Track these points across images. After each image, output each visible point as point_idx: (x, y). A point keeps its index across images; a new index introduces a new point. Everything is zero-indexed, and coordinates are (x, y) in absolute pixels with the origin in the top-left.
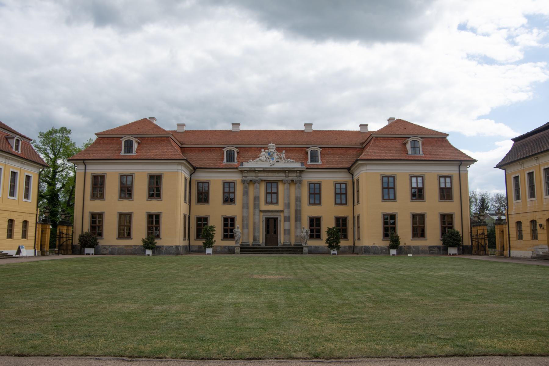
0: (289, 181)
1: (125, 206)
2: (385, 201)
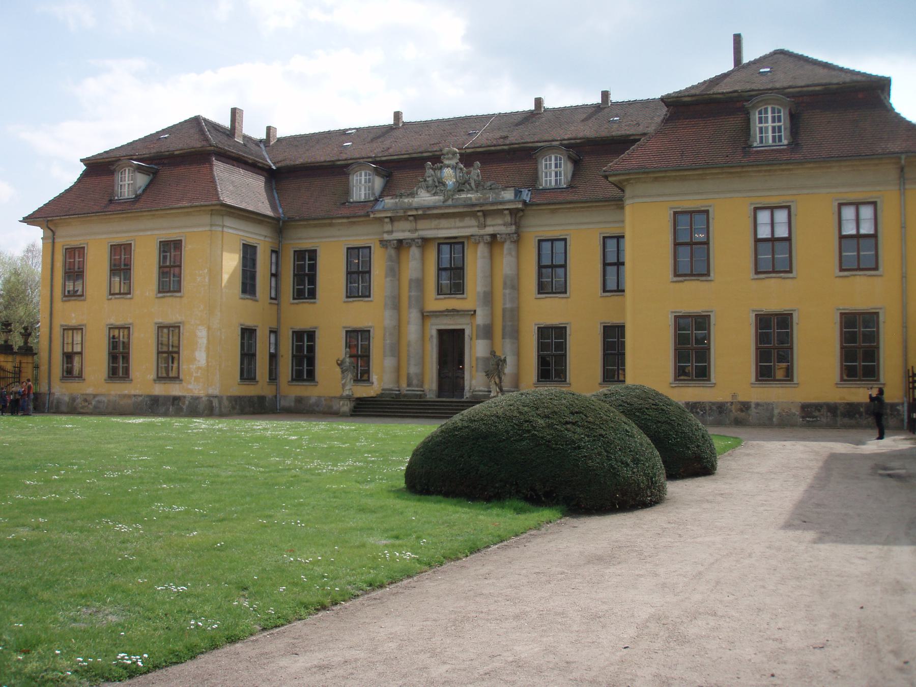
2: (680, 279)
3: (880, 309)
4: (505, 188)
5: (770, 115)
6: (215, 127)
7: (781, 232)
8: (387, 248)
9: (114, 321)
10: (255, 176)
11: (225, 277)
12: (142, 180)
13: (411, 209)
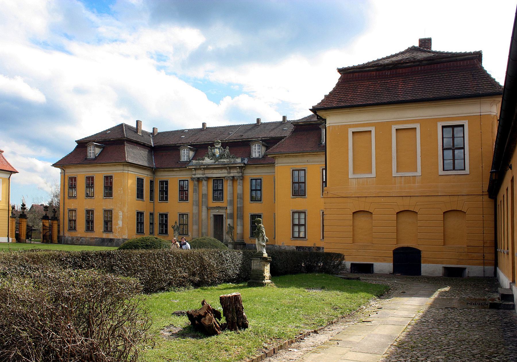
2: (295, 197)
6: (129, 128)
12: (98, 151)
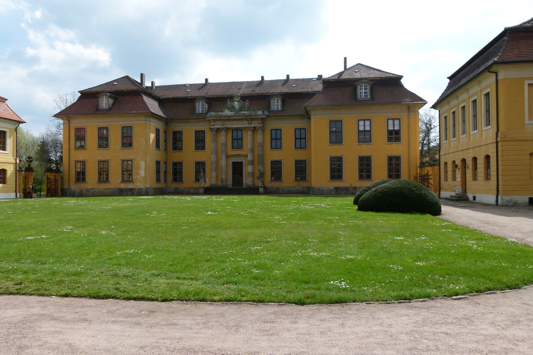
0: (251, 128)
1: (103, 154)
2: (332, 144)
3: (401, 155)
4: (259, 110)
5: (364, 87)
7: (368, 128)
8: (212, 131)
9: (100, 158)
10: (155, 101)
11: (151, 141)
12: (111, 101)
13: (223, 117)
